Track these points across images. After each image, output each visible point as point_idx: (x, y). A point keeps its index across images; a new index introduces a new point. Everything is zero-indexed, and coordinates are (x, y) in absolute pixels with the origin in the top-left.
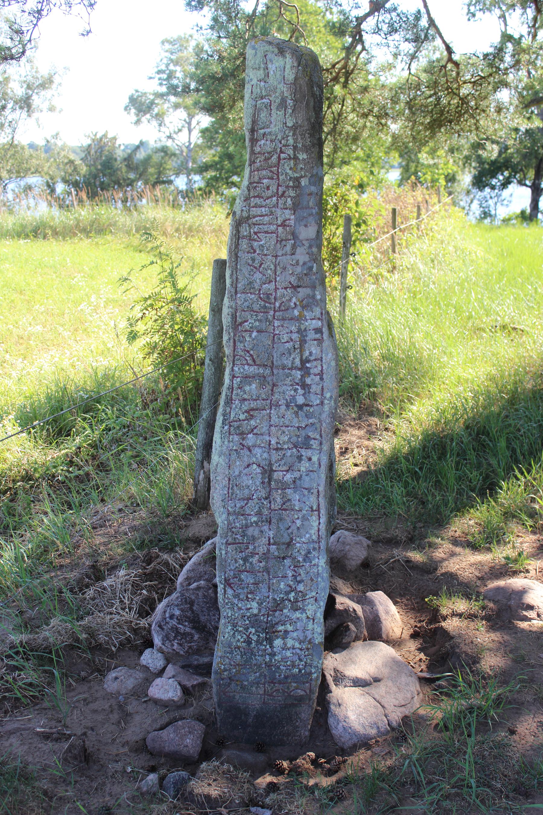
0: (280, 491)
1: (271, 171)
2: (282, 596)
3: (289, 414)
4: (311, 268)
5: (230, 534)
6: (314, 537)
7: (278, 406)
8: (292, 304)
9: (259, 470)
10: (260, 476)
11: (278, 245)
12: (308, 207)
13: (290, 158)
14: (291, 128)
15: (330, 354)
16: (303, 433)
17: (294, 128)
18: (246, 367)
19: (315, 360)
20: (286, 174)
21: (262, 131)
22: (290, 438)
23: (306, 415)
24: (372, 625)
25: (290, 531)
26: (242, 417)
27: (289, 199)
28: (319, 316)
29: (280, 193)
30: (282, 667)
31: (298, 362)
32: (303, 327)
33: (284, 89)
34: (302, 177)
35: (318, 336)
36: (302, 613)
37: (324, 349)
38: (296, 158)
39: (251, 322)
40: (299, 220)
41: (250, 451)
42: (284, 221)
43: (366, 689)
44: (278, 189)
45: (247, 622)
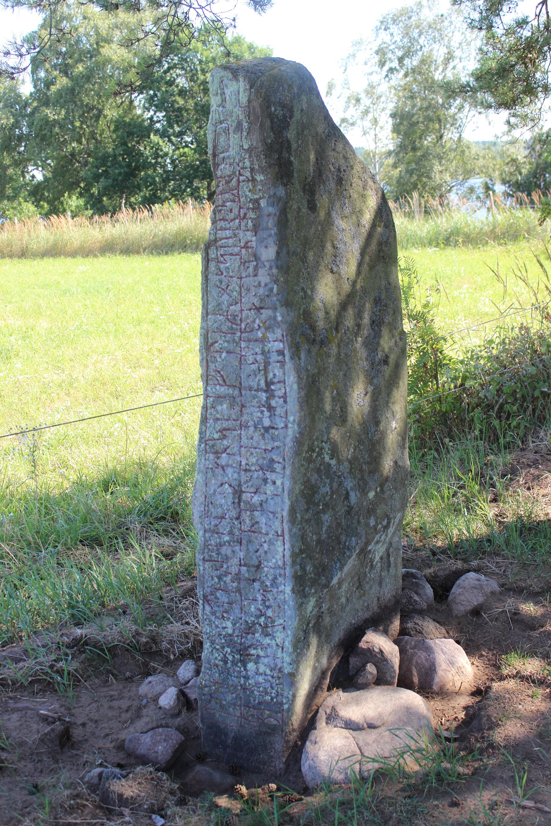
0: (248, 513)
1: (233, 194)
2: (253, 619)
3: (257, 436)
4: (271, 290)
5: (206, 551)
6: (280, 563)
7: (247, 427)
8: (256, 326)
9: (230, 490)
10: (231, 496)
11: (242, 267)
12: (267, 229)
13: (249, 180)
14: (247, 151)
15: (292, 377)
16: (268, 456)
17: (250, 150)
18: (218, 387)
19: (279, 382)
20: (246, 196)
21: (222, 156)
22: (257, 460)
23: (272, 438)
24: (427, 674)
25: (258, 554)
26: (216, 436)
27: (250, 221)
28: (280, 338)
29: (242, 215)
30: (255, 692)
31: (263, 384)
32: (266, 349)
33: (239, 113)
34: (260, 198)
35: (280, 358)
36: (271, 640)
37: (286, 370)
38: (254, 180)
39: (221, 343)
40: (261, 241)
41: (224, 470)
42: (247, 243)
43: (355, 733)
44: (239, 212)
45: (223, 641)
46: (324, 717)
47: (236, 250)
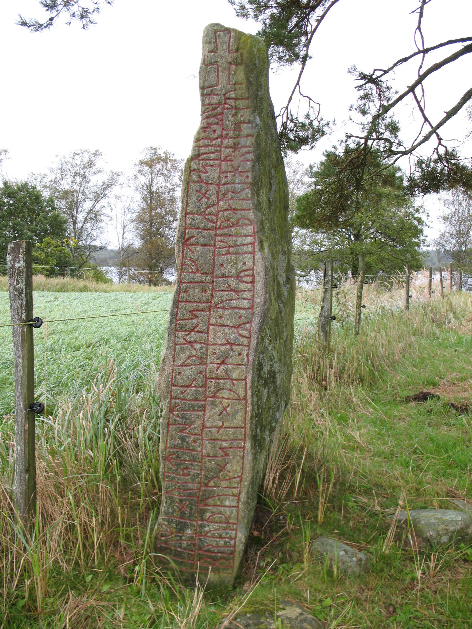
1: (217, 119)
44: (222, 132)
46: (236, 554)
47: (217, 162)
